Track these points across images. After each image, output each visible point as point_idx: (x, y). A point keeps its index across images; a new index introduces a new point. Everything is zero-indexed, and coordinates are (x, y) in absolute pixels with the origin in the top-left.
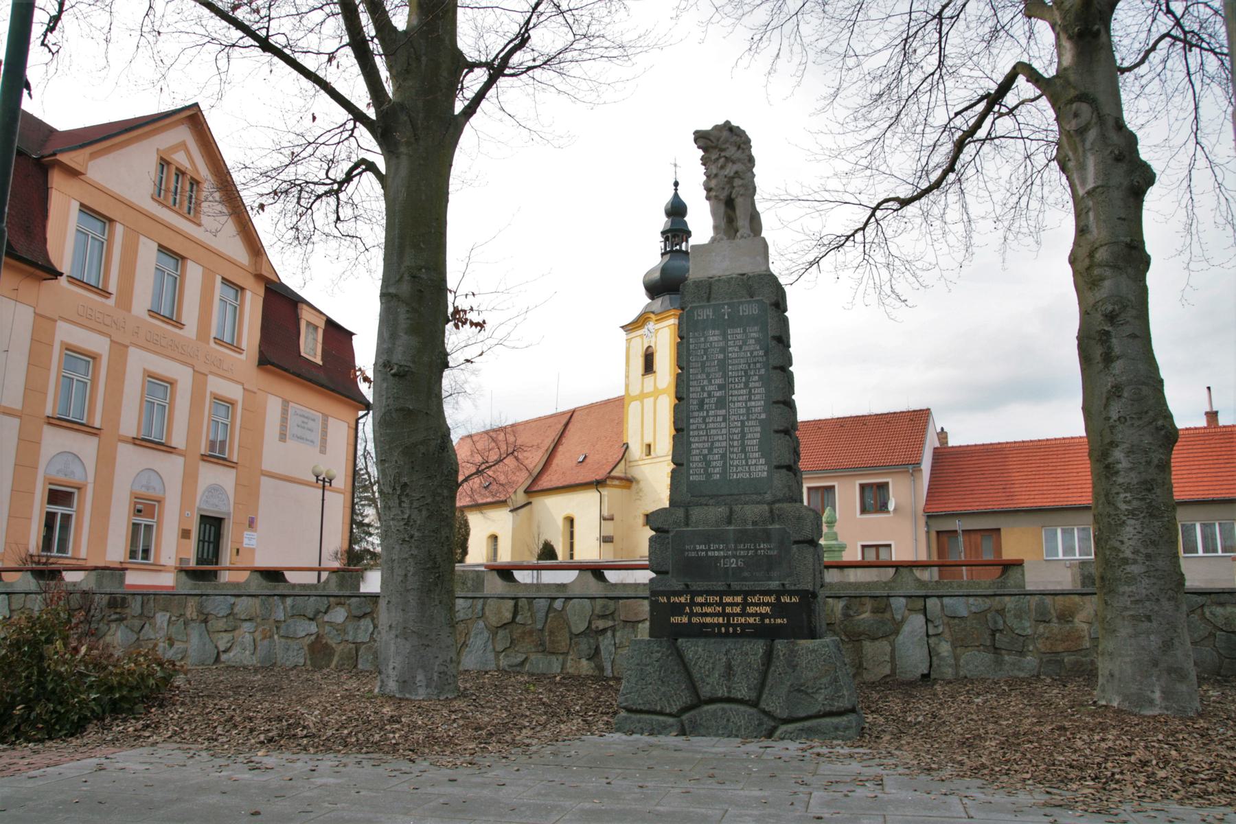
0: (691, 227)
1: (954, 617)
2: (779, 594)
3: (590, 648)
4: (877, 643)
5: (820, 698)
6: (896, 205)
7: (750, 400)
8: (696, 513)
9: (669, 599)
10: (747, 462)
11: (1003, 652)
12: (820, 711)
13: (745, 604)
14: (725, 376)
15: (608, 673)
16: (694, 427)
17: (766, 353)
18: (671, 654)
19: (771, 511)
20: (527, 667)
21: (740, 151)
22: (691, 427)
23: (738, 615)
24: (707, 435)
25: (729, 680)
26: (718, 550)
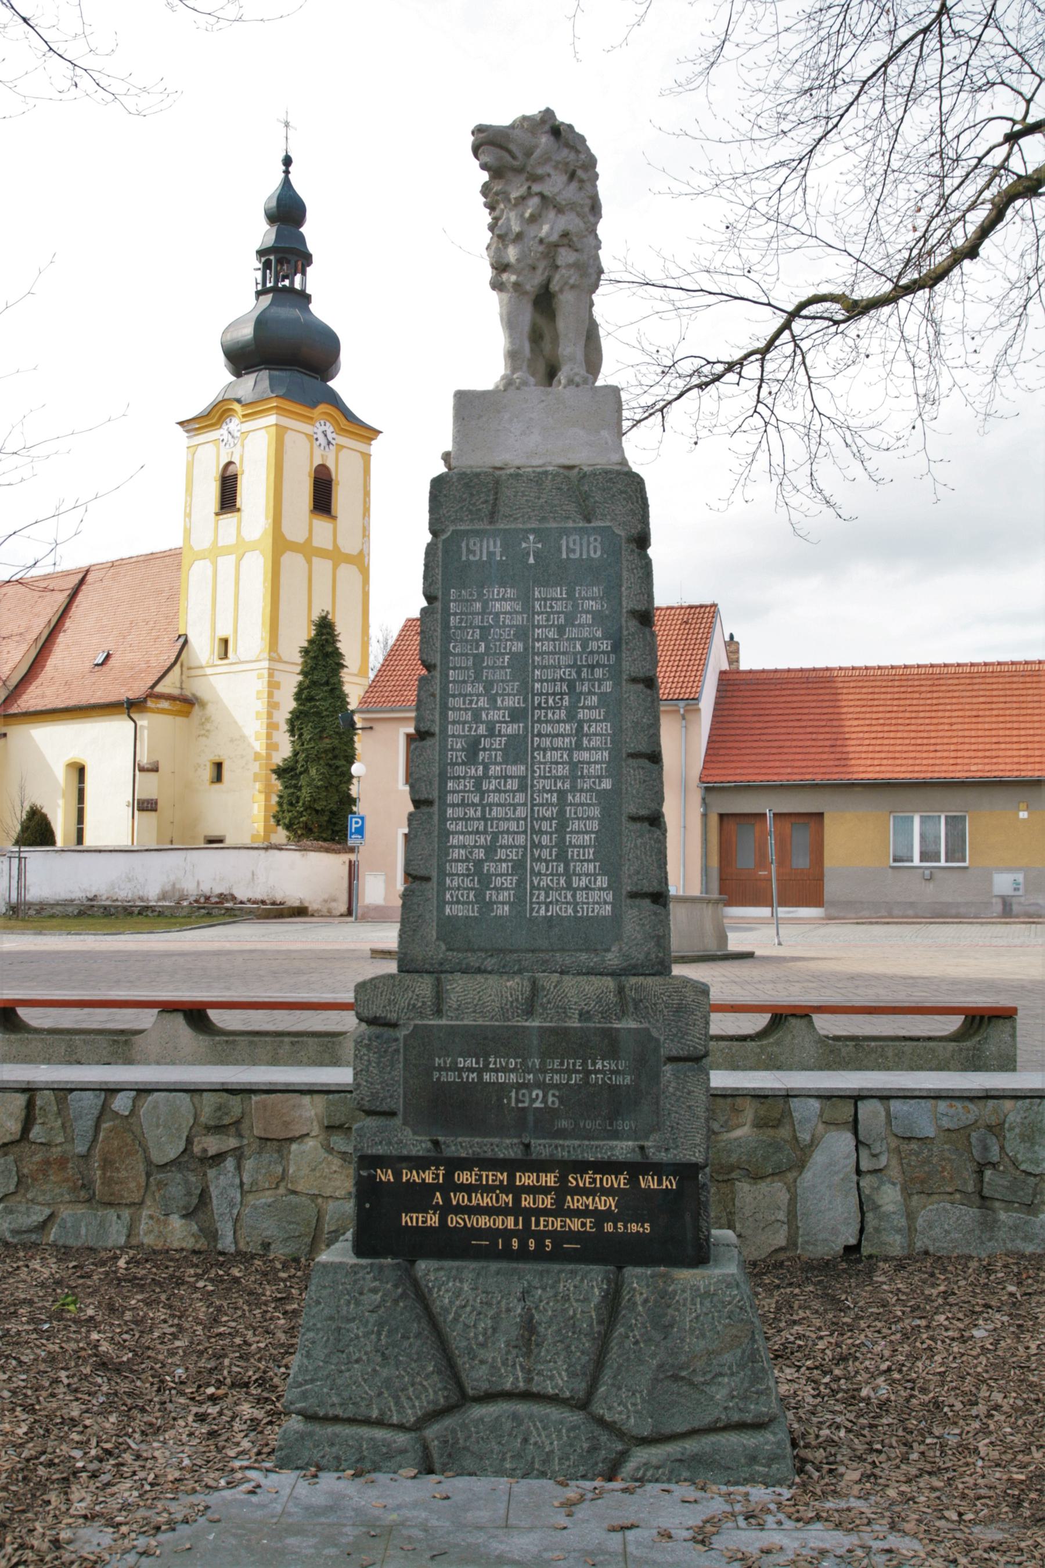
0: (311, 246)
1: (909, 1139)
2: (635, 1169)
3: (189, 1194)
4: (763, 1186)
5: (720, 1395)
6: (836, 310)
7: (579, 747)
8: (459, 987)
9: (398, 1175)
10: (569, 883)
11: (997, 1204)
12: (719, 1419)
13: (562, 1191)
14: (525, 690)
15: (227, 1243)
16: (455, 799)
17: (616, 648)
18: (403, 1296)
19: (621, 990)
20: (53, 1234)
21: (574, 185)
22: (450, 799)
23: (546, 1212)
24: (483, 818)
25: (528, 1354)
26: (505, 1070)
